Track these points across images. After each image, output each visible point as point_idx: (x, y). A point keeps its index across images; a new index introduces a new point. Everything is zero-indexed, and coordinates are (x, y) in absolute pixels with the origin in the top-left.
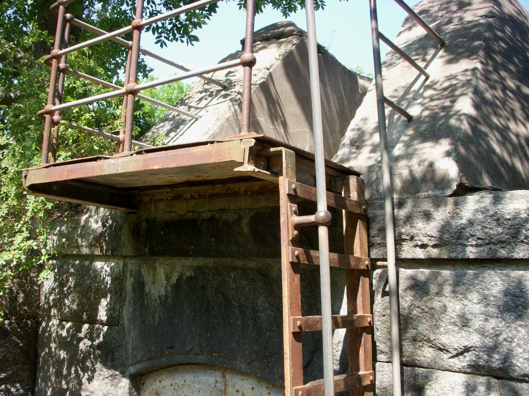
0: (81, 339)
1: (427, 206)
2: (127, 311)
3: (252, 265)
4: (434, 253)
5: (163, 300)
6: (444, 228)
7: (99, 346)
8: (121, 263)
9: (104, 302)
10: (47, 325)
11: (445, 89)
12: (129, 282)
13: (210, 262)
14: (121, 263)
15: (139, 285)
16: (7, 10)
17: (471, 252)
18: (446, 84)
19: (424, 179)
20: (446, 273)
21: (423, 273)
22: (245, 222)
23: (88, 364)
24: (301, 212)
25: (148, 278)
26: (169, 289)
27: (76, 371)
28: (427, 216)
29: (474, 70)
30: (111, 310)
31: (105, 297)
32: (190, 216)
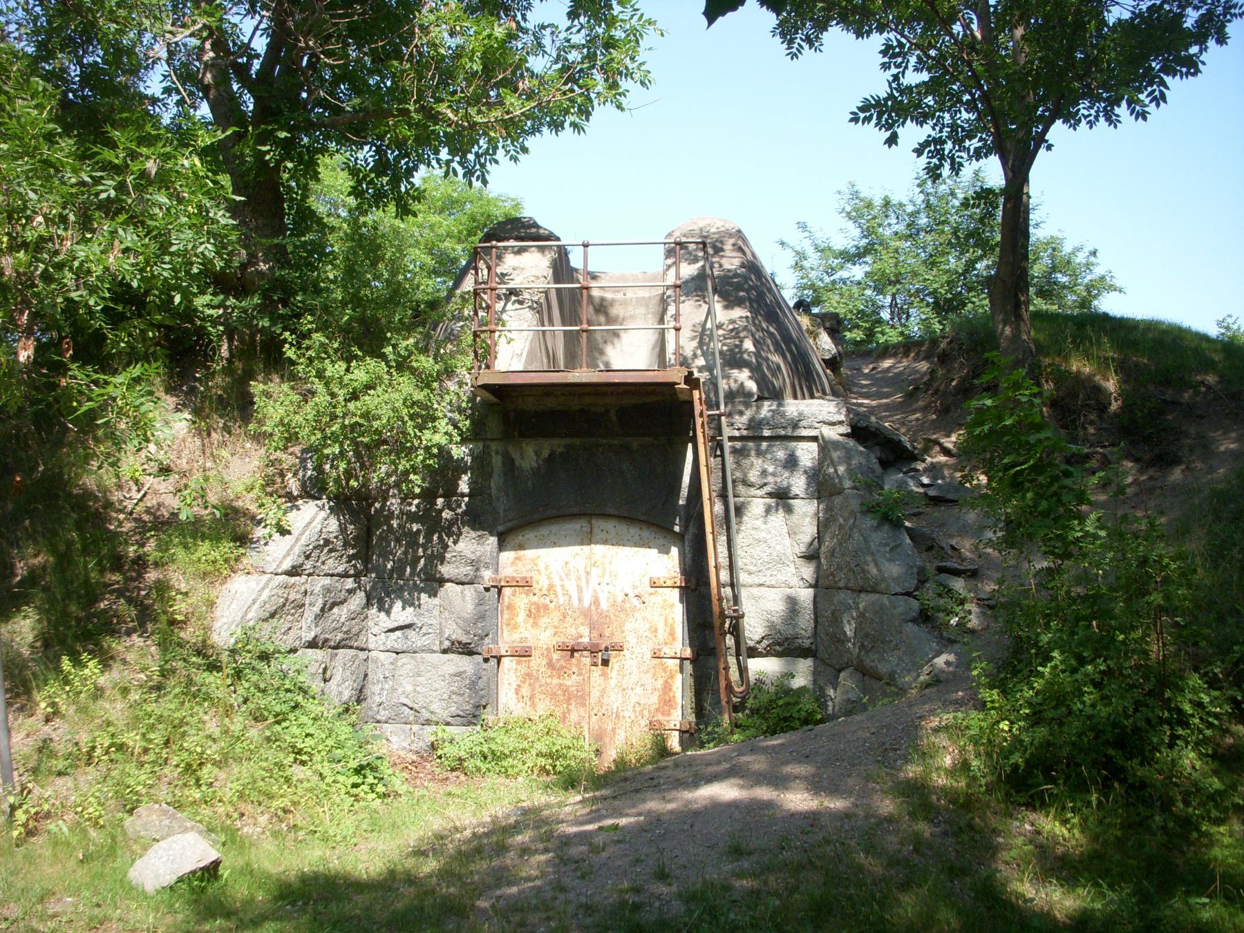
0: (441, 511)
1: (742, 408)
2: (495, 483)
3: (616, 442)
4: (745, 433)
5: (536, 471)
6: (751, 420)
7: (465, 513)
8: (481, 445)
9: (465, 478)
10: (384, 505)
11: (732, 331)
12: (497, 461)
13: (577, 441)
14: (481, 445)
15: (509, 462)
16: (1013, 425)
17: (766, 433)
18: (731, 327)
19: (738, 391)
20: (751, 444)
21: (738, 445)
22: (612, 412)
23: (455, 529)
24: (710, 407)
25: (515, 454)
26: (541, 462)
27: (440, 538)
28: (741, 413)
29: (747, 317)
30: (471, 483)
31: (466, 473)
32: (560, 408)
